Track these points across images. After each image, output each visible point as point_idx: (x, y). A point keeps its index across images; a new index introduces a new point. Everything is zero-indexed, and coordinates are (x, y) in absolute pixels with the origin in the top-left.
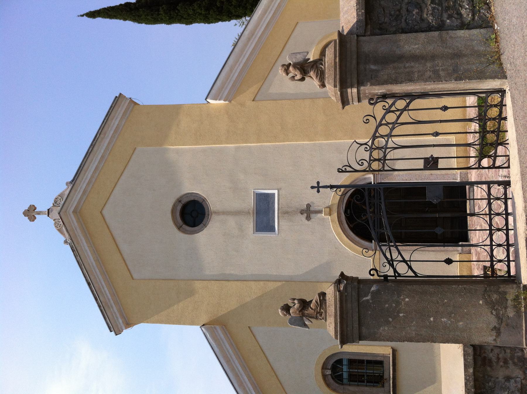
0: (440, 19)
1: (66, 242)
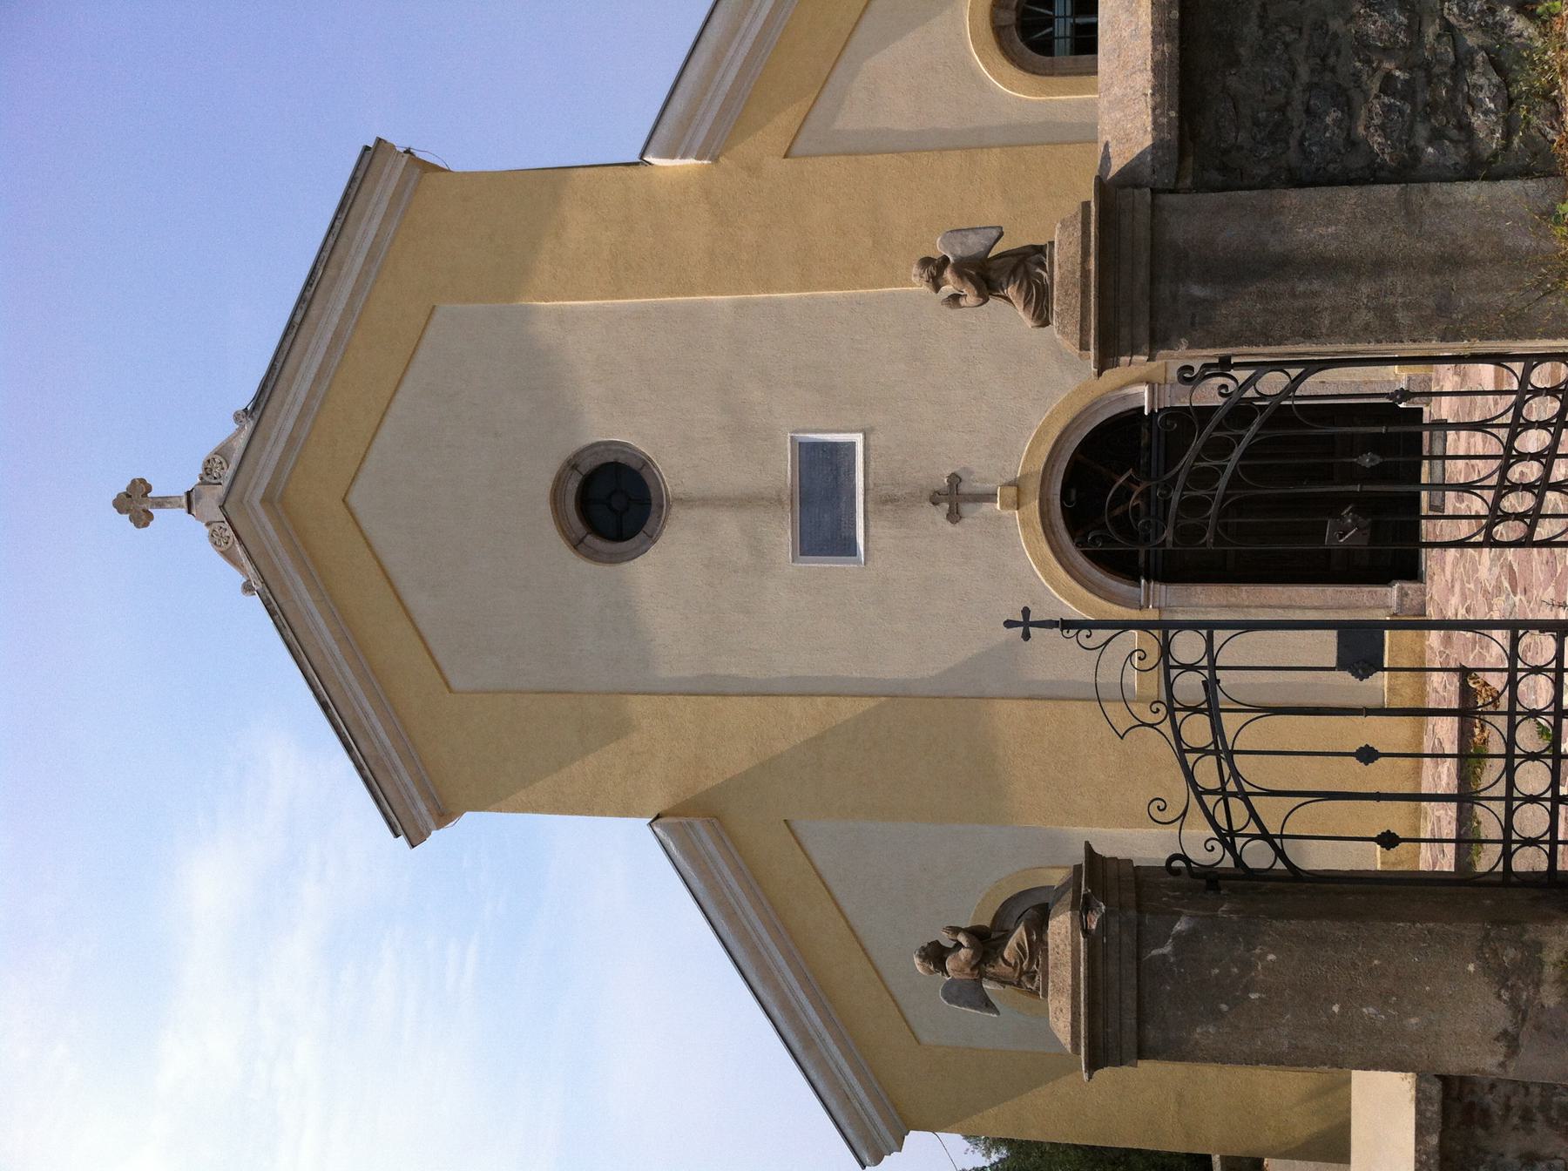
0: (1407, 142)
1: (247, 588)
